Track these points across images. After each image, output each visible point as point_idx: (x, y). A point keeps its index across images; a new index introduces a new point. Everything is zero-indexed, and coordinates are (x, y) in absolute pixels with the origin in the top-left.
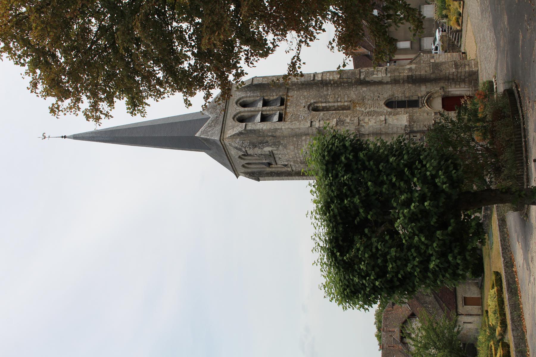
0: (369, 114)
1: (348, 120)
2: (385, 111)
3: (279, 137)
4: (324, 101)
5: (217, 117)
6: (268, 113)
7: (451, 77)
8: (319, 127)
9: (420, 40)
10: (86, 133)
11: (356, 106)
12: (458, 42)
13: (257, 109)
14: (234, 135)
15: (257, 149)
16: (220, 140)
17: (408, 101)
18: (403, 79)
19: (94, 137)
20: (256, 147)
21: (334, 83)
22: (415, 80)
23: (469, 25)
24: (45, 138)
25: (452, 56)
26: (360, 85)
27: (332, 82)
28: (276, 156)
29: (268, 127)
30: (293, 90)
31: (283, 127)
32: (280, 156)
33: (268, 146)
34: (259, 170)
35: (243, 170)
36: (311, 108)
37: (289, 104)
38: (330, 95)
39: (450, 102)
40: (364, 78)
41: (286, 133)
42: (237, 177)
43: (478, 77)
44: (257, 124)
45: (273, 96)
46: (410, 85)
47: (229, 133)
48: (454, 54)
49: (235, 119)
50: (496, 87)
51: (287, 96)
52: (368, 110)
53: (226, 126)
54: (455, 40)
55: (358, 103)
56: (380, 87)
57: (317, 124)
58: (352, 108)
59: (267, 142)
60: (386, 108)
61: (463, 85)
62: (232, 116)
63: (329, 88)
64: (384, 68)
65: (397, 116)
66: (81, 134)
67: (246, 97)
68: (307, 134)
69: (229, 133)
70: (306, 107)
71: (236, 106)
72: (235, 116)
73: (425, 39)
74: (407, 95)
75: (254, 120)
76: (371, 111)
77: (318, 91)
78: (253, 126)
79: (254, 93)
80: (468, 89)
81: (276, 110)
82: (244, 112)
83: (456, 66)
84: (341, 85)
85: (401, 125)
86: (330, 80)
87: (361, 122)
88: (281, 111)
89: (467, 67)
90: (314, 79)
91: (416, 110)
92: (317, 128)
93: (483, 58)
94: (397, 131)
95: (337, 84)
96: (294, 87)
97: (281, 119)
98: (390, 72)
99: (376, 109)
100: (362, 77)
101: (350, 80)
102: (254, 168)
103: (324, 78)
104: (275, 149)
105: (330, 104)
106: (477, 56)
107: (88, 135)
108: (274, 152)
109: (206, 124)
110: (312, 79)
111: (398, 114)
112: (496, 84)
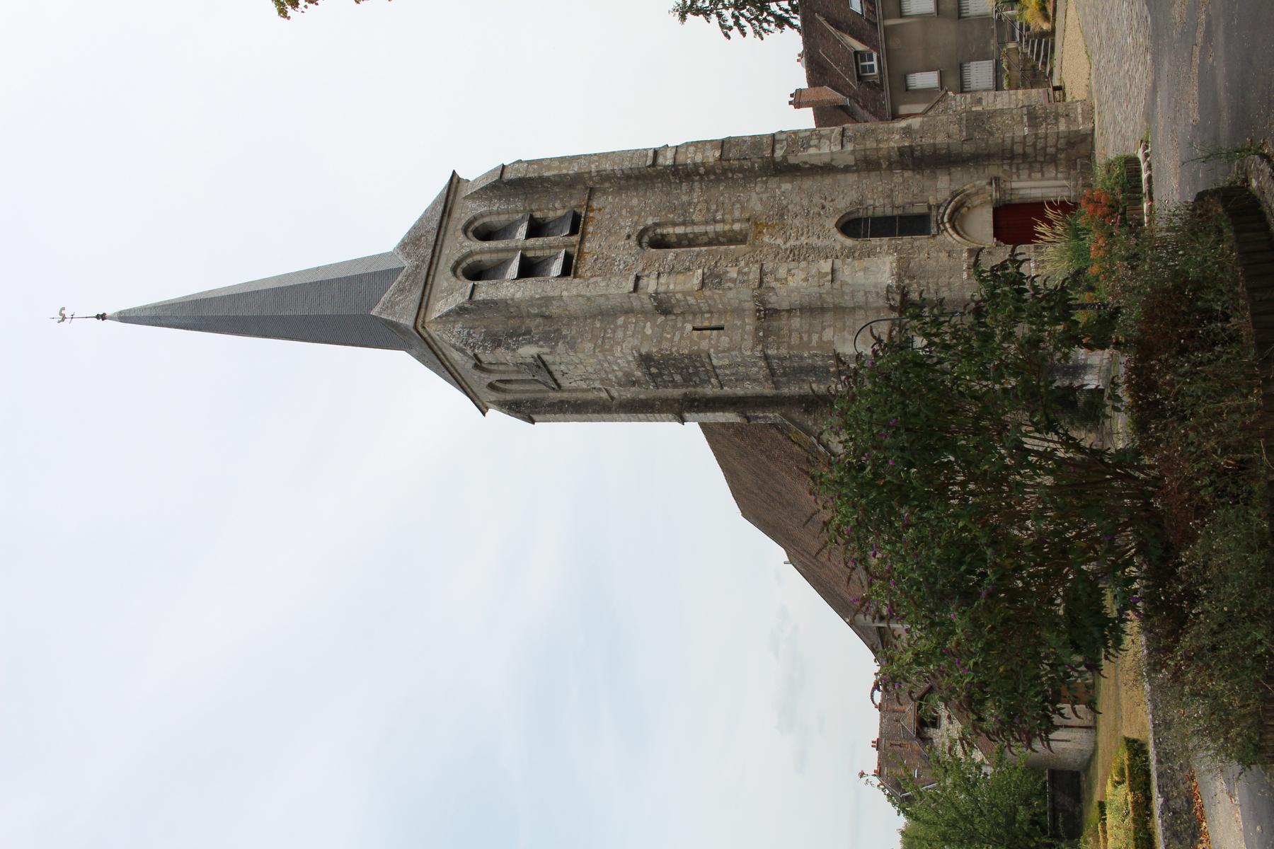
0: (796, 255)
1: (733, 273)
2: (838, 247)
3: (560, 318)
4: (681, 220)
5: (417, 266)
6: (539, 253)
7: (1018, 149)
8: (656, 293)
9: (961, 67)
11: (761, 232)
12: (1044, 64)
13: (512, 244)
14: (448, 314)
15: (501, 350)
16: (415, 327)
17: (901, 217)
18: (889, 158)
21: (707, 173)
22: (920, 160)
23: (1071, 13)
24: (64, 318)
25: (1029, 97)
26: (775, 176)
27: (702, 170)
28: (552, 368)
29: (528, 294)
30: (605, 193)
31: (565, 294)
32: (563, 367)
33: (529, 342)
35: (494, 396)
36: (646, 239)
37: (590, 229)
38: (696, 205)
39: (1016, 222)
40: (784, 157)
41: (574, 308)
43: (1093, 147)
44: (509, 287)
45: (554, 210)
46: (908, 174)
47: (440, 307)
48: (1034, 91)
49: (459, 271)
50: (1150, 178)
51: (589, 208)
52: (792, 243)
53: (434, 291)
54: (1038, 59)
55: (767, 225)
56: (828, 181)
58: (750, 238)
59: (528, 332)
60: (840, 237)
61: (1051, 172)
62: (452, 262)
63: (697, 185)
64: (837, 129)
65: (866, 262)
66: (134, 310)
67: (491, 213)
68: (629, 311)
69: (440, 307)
70: (634, 237)
72: (458, 263)
73: (973, 65)
74: (899, 201)
75: (504, 274)
76: (801, 247)
77: (668, 194)
78: (492, 291)
80: (1065, 182)
81: (559, 247)
82: (482, 252)
83: (1033, 117)
84: (727, 177)
85: (875, 286)
86: (696, 165)
87: (769, 279)
88: (571, 250)
89: (1062, 121)
90: (654, 163)
91: (921, 240)
92: (651, 296)
93: (1107, 91)
94: (866, 302)
95: (715, 173)
96: (607, 185)
97: (567, 271)
98: (853, 139)
99: (814, 241)
100: (779, 153)
101: (747, 164)
102: (518, 392)
103: (681, 159)
104: (546, 350)
105: (697, 229)
106: (1090, 92)
107: (148, 314)
108: (545, 358)
111: (870, 254)
112: (1149, 167)
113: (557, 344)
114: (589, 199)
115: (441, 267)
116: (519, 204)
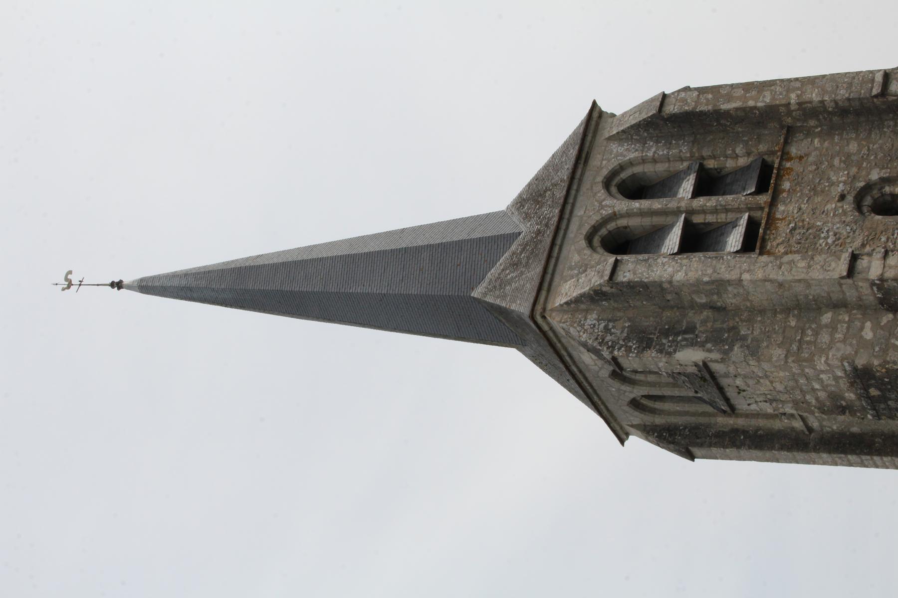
3: (737, 311)
5: (538, 232)
6: (710, 218)
8: (882, 279)
10: (174, 275)
13: (672, 204)
14: (578, 300)
16: (532, 316)
19: (190, 289)
20: (648, 347)
24: (70, 285)
28: (724, 382)
29: (693, 276)
30: (809, 133)
31: (746, 277)
32: (739, 382)
33: (693, 344)
34: (692, 420)
35: (637, 418)
36: (868, 201)
37: (786, 185)
41: (758, 297)
42: (622, 442)
44: (666, 265)
45: (737, 157)
47: (568, 289)
49: (596, 241)
51: (785, 156)
53: (560, 267)
57: (873, 267)
59: (691, 329)
62: (586, 228)
69: (568, 289)
70: (850, 198)
71: (602, 193)
72: (595, 229)
79: (669, 145)
81: (739, 211)
82: (629, 214)
88: (757, 214)
92: (873, 284)
96: (812, 123)
97: (750, 244)
102: (673, 414)
104: (715, 356)
109: (507, 255)
110: (876, 90)
113: (731, 349)
114: (786, 142)
115: (571, 235)
116: (684, 149)
